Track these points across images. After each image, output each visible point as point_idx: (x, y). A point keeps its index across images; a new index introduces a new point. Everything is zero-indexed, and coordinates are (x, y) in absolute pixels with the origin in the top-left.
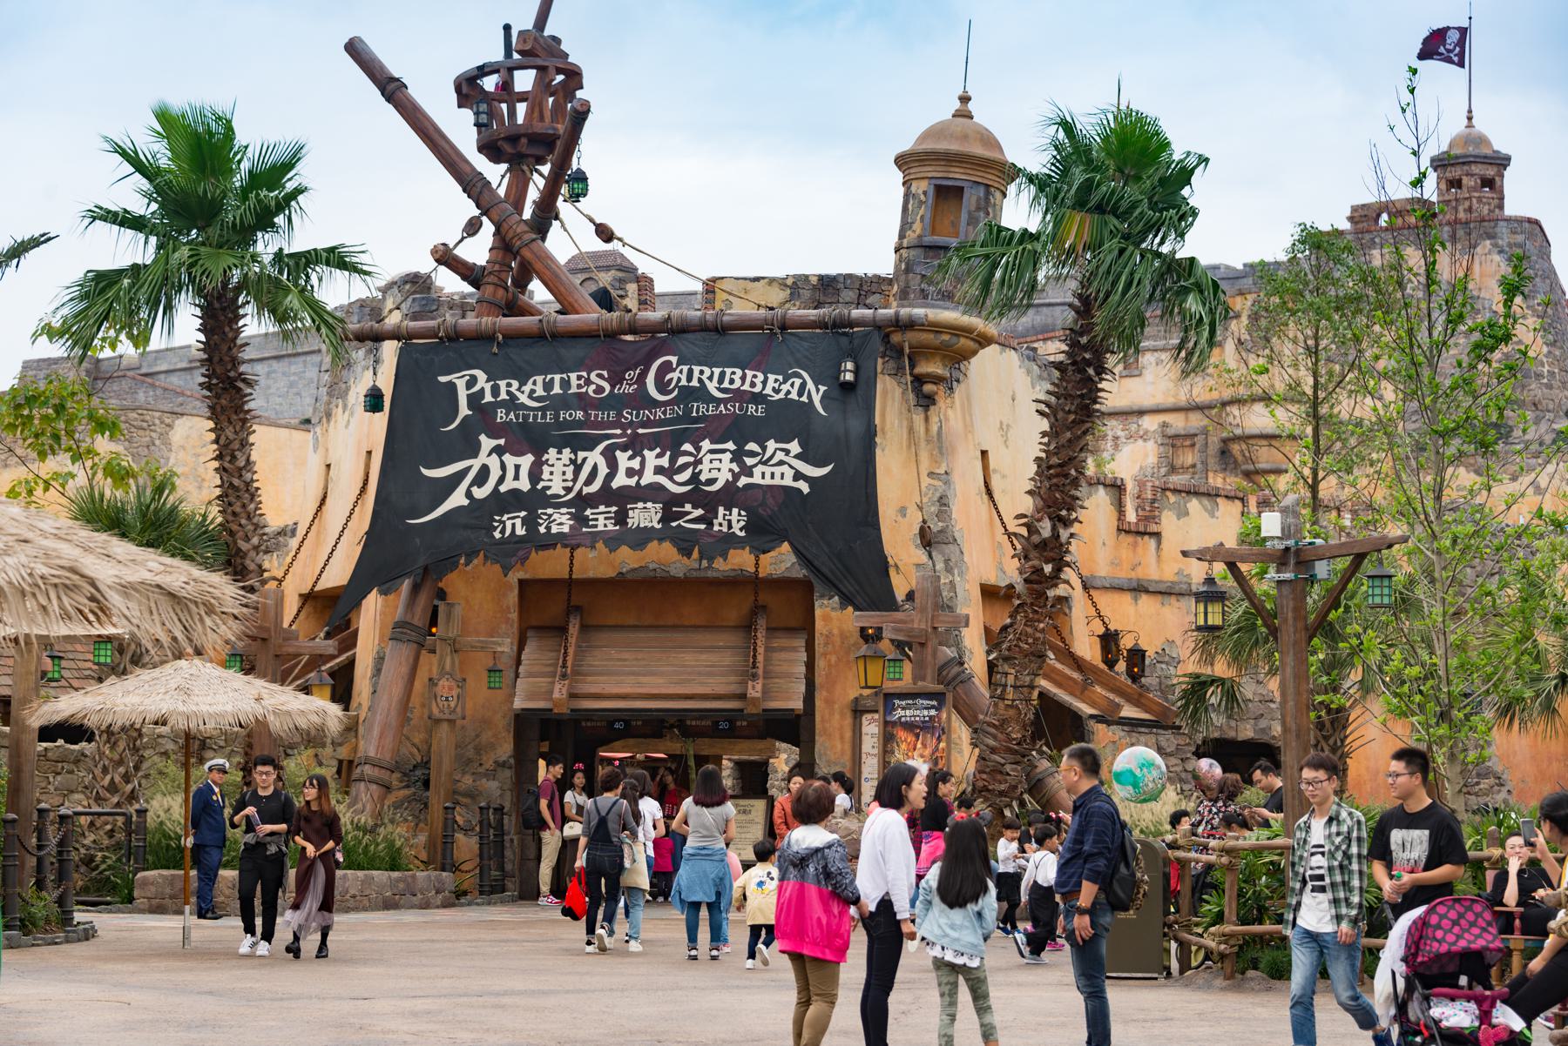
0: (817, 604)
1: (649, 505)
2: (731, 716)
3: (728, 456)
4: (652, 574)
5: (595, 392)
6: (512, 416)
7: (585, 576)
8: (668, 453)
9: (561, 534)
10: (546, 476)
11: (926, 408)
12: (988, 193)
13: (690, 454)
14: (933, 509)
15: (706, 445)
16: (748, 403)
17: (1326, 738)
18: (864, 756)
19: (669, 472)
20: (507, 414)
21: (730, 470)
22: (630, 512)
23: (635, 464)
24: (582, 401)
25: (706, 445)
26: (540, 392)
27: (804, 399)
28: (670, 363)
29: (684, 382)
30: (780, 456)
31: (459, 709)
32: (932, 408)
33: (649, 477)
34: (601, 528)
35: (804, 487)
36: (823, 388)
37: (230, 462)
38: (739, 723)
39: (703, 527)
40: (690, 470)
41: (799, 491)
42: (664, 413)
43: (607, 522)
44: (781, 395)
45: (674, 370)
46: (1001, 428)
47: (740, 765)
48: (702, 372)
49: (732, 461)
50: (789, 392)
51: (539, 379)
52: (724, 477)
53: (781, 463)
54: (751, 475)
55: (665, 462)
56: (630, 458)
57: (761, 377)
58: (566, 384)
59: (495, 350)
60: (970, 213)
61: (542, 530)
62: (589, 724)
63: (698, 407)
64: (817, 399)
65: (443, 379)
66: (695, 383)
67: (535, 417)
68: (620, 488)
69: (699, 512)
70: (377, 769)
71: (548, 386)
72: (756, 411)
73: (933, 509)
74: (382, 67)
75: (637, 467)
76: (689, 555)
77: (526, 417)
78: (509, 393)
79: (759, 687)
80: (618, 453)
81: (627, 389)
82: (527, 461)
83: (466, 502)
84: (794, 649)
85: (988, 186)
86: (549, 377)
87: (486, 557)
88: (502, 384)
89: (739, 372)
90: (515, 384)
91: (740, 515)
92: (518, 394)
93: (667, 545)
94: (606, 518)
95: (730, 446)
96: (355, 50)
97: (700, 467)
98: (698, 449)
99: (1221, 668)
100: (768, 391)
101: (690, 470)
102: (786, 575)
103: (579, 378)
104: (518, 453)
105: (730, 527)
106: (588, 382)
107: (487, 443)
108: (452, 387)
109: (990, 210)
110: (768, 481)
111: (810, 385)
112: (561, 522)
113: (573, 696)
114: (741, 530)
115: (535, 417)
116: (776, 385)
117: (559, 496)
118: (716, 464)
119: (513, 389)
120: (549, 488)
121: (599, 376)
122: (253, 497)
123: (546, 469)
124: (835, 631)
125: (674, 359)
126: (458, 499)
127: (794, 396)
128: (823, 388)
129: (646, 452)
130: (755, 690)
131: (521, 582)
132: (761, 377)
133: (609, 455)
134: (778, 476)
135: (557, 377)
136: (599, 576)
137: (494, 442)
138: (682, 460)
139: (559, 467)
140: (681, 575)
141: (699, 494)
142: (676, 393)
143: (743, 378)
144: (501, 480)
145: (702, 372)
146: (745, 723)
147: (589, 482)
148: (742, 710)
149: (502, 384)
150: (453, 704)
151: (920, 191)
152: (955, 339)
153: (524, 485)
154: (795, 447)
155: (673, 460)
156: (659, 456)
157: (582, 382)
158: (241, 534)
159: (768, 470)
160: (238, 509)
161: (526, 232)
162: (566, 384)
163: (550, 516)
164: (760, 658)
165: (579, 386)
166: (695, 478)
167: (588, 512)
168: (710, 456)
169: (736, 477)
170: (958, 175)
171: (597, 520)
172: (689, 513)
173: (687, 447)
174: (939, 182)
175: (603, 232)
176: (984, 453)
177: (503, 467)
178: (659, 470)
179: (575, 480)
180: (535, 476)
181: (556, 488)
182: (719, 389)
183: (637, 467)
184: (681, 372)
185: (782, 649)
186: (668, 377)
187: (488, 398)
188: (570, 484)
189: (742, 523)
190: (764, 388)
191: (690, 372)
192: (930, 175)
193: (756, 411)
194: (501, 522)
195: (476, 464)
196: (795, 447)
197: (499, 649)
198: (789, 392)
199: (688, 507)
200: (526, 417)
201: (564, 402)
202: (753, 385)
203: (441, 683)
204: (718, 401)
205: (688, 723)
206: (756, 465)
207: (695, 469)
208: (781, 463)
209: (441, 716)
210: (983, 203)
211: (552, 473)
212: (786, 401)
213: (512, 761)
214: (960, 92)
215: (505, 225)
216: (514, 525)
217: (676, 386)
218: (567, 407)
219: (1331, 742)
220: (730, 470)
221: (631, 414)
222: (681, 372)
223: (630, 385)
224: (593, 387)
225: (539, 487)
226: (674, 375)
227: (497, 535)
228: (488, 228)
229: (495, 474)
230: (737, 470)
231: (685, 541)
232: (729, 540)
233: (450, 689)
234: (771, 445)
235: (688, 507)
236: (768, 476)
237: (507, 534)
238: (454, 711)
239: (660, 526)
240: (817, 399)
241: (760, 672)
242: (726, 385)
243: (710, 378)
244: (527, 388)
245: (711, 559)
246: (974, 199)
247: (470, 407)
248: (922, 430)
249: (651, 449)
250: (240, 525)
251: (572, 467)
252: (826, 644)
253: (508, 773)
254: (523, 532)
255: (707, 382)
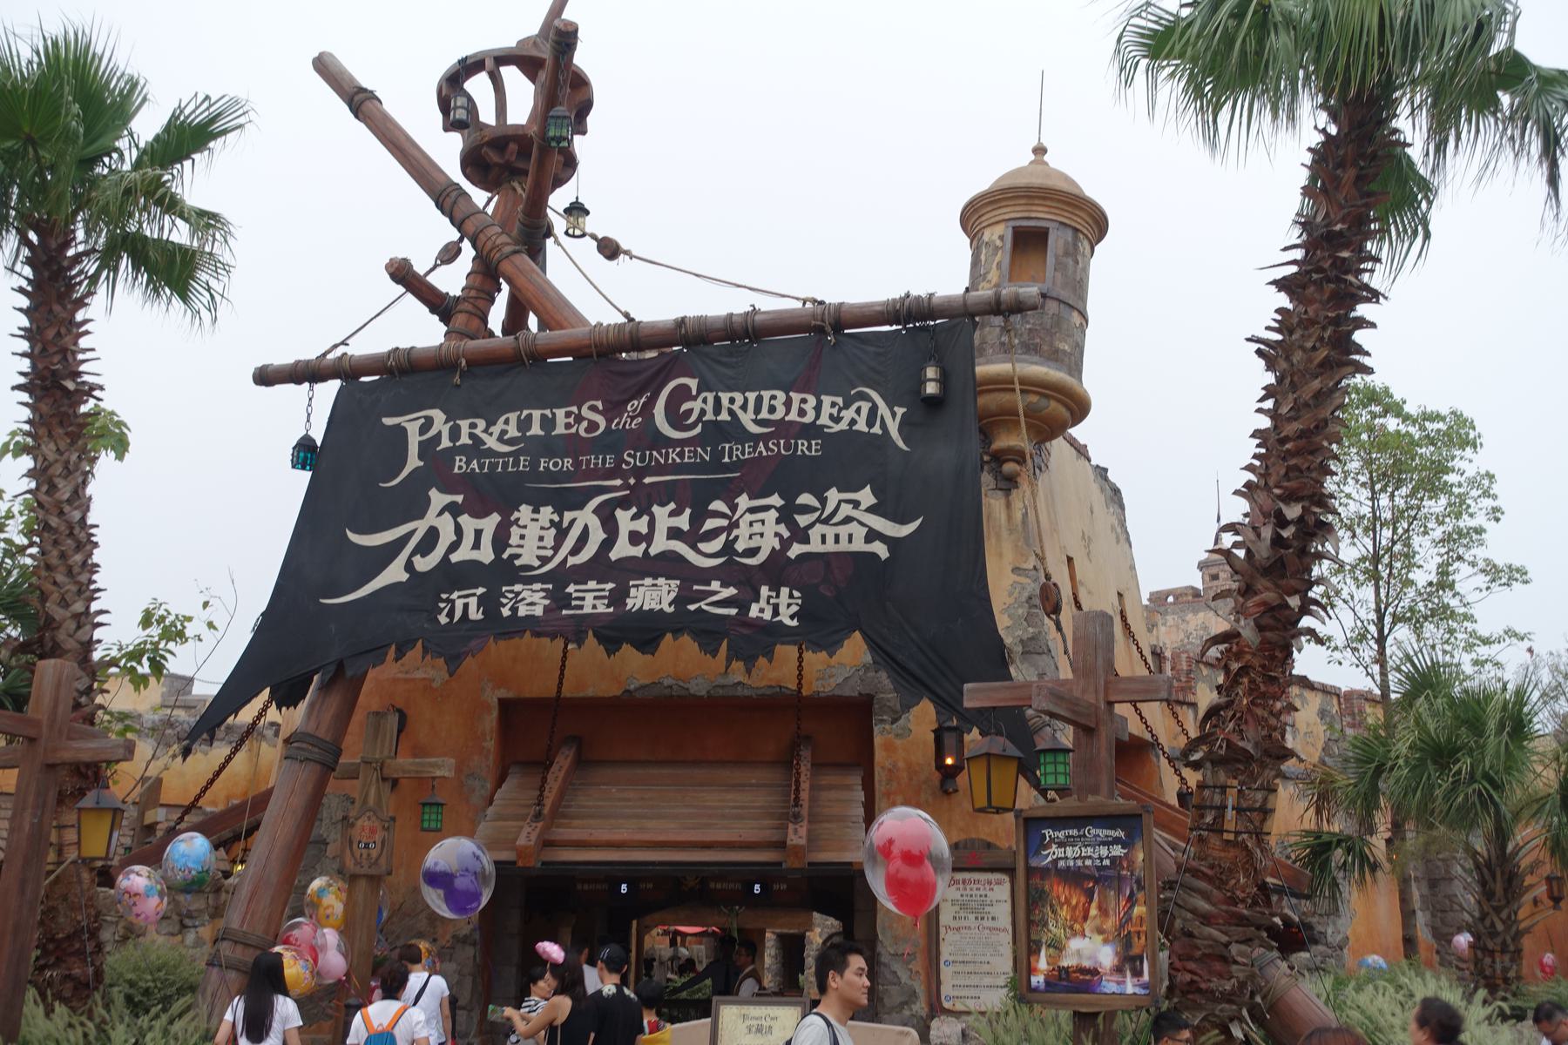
0: (876, 729)
1: (661, 581)
2: (764, 873)
3: (773, 514)
4: (667, 692)
5: (587, 430)
6: (475, 464)
7: (581, 695)
8: (688, 511)
9: (530, 618)
10: (514, 540)
11: (1007, 492)
12: (1076, 239)
13: (722, 515)
14: (1020, 611)
15: (743, 501)
16: (796, 439)
17: (1498, 910)
18: (942, 930)
19: (693, 537)
20: (468, 463)
21: (777, 534)
22: (633, 591)
23: (642, 526)
24: (572, 445)
25: (743, 501)
26: (513, 432)
27: (877, 430)
28: (687, 388)
29: (709, 416)
30: (846, 510)
31: (383, 861)
32: (1014, 492)
33: (660, 544)
34: (588, 610)
35: (881, 550)
36: (900, 411)
37: (47, 493)
38: (776, 887)
39: (733, 611)
40: (723, 537)
41: (874, 556)
42: (681, 455)
43: (598, 602)
44: (843, 426)
45: (695, 398)
46: (1083, 537)
47: (781, 938)
48: (732, 401)
49: (778, 521)
50: (853, 422)
51: (513, 416)
52: (769, 544)
53: (848, 520)
54: (806, 541)
55: (683, 522)
56: (635, 517)
57: (812, 401)
58: (548, 423)
59: (457, 380)
60: (1057, 257)
61: (506, 612)
62: (586, 887)
63: (731, 448)
64: (893, 428)
65: (388, 421)
66: (724, 416)
67: (505, 465)
68: (619, 560)
69: (732, 591)
70: (239, 948)
71: (524, 424)
72: (809, 448)
73: (1020, 611)
74: (343, 72)
75: (644, 530)
76: (714, 653)
77: (493, 466)
78: (472, 436)
79: (803, 831)
80: (619, 513)
81: (628, 421)
82: (490, 523)
83: (405, 577)
84: (848, 788)
85: (1076, 230)
86: (525, 412)
87: (425, 650)
88: (464, 424)
89: (781, 395)
90: (481, 424)
91: (791, 596)
92: (484, 436)
93: (686, 639)
94: (595, 598)
95: (776, 500)
96: (325, 67)
97: (735, 532)
98: (734, 508)
99: (1339, 825)
100: (824, 420)
101: (723, 537)
102: (838, 692)
103: (568, 415)
104: (479, 514)
105: (776, 612)
106: (579, 419)
107: (438, 499)
108: (401, 432)
109: (1080, 259)
110: (830, 547)
111: (883, 409)
112: (532, 601)
113: (548, 844)
114: (792, 617)
115: (505, 465)
116: (835, 411)
117: (531, 568)
118: (757, 528)
119: (478, 431)
120: (518, 556)
121: (593, 409)
122: (79, 546)
123: (515, 530)
124: (901, 764)
125: (693, 384)
126: (394, 573)
127: (861, 426)
128: (900, 411)
129: (656, 509)
130: (797, 836)
131: (503, 703)
132: (812, 401)
133: (607, 517)
134: (844, 539)
135: (537, 414)
136: (600, 694)
137: (448, 499)
138: (710, 524)
139: (533, 531)
140: (703, 693)
141: (732, 569)
142: (698, 429)
143: (788, 404)
144: (454, 547)
145: (732, 401)
146: (784, 887)
147: (575, 551)
148: (780, 864)
149: (464, 424)
150: (374, 854)
151: (995, 237)
152: (1044, 402)
153: (486, 555)
154: (866, 496)
155: (696, 521)
156: (674, 514)
157: (571, 420)
158: (56, 596)
159: (830, 532)
160: (54, 561)
161: (508, 244)
162: (548, 423)
163: (518, 594)
164: (804, 795)
165: (568, 426)
166: (728, 548)
167: (571, 589)
168: (749, 517)
169: (786, 544)
170: (1040, 215)
171: (583, 599)
172: (715, 593)
173: (718, 505)
174: (1018, 223)
175: (606, 247)
176: (1070, 560)
177: (459, 531)
178: (674, 533)
179: (556, 548)
180: (500, 541)
181: (528, 557)
182: (757, 422)
183: (644, 530)
184: (705, 401)
185: (830, 788)
186: (685, 407)
187: (446, 443)
188: (549, 553)
189: (795, 609)
190: (818, 416)
191: (717, 401)
192: (1007, 217)
193: (809, 448)
194: (448, 601)
195: (420, 527)
196: (866, 496)
197: (438, 773)
198: (853, 422)
199: (715, 585)
200: (493, 466)
201: (549, 445)
202: (802, 413)
203: (359, 823)
204: (756, 438)
205: (712, 885)
206: (812, 525)
207: (729, 535)
208: (848, 520)
209: (358, 870)
210: (1071, 249)
211: (522, 537)
212: (851, 434)
213: (477, 936)
214: (1035, 143)
215: (481, 236)
216: (466, 606)
217: (699, 419)
218: (551, 454)
219: (1504, 915)
220: (777, 534)
221: (634, 457)
222: (705, 401)
223: (633, 418)
224: (585, 424)
225: (505, 556)
226: (696, 406)
227: (443, 619)
228: (468, 251)
229: (447, 536)
230: (786, 534)
231: (708, 632)
232: (772, 632)
233: (373, 831)
234: (833, 495)
235: (715, 585)
236: (830, 539)
237: (456, 619)
238: (376, 862)
239: (672, 609)
240: (893, 428)
241: (805, 811)
242: (764, 415)
243: (744, 407)
244: (496, 430)
245: (750, 661)
246: (1061, 242)
247: (420, 457)
248: (1003, 517)
249: (663, 504)
250: (55, 583)
251: (553, 531)
252: (889, 781)
253: (470, 951)
254: (480, 616)
255: (740, 413)
